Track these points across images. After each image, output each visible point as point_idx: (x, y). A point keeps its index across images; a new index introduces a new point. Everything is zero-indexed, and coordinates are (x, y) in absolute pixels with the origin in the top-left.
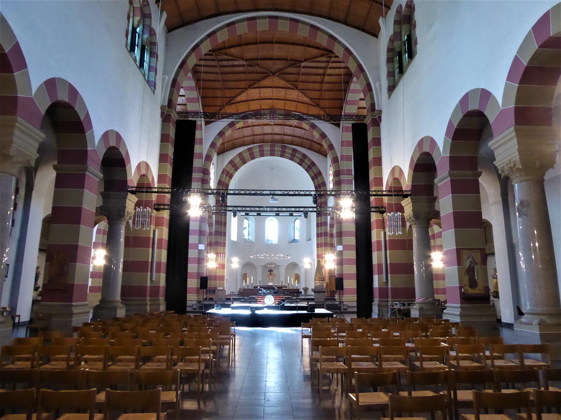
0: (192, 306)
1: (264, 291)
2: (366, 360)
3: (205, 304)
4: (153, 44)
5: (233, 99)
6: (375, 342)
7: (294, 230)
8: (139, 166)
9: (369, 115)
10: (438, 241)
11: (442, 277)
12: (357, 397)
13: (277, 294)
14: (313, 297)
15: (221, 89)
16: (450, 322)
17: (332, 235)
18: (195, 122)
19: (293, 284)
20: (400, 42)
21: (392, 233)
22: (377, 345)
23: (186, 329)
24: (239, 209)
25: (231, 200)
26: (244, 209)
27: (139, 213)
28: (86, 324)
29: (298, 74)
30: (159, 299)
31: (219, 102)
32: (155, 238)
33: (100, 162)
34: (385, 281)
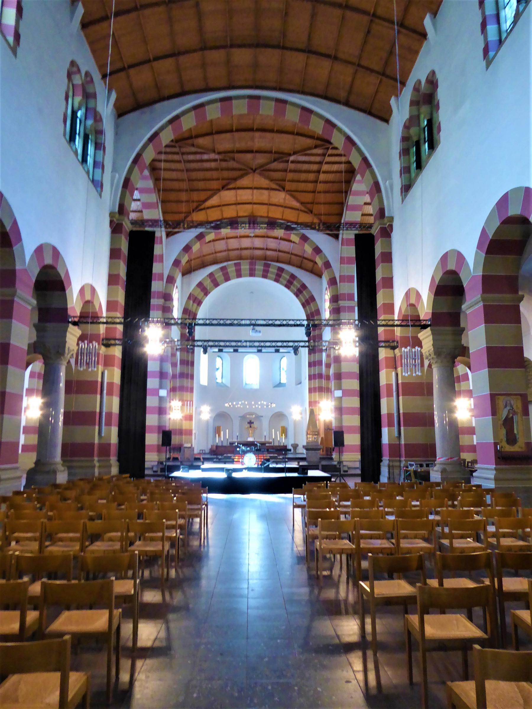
0: (152, 468)
1: (243, 448)
2: (378, 537)
3: (168, 466)
4: (99, 132)
6: (388, 513)
8: (82, 291)
9: (377, 223)
10: (463, 386)
11: (471, 431)
12: (372, 587)
13: (260, 452)
14: (305, 456)
15: (187, 190)
16: (483, 488)
17: (328, 378)
18: (153, 233)
19: (279, 439)
20: (418, 128)
21: (409, 373)
22: (392, 518)
23: (145, 497)
24: (211, 344)
25: (199, 333)
26: (217, 344)
27: (83, 349)
28: (18, 493)
29: (285, 171)
30: (110, 460)
31: (184, 208)
33: (32, 285)
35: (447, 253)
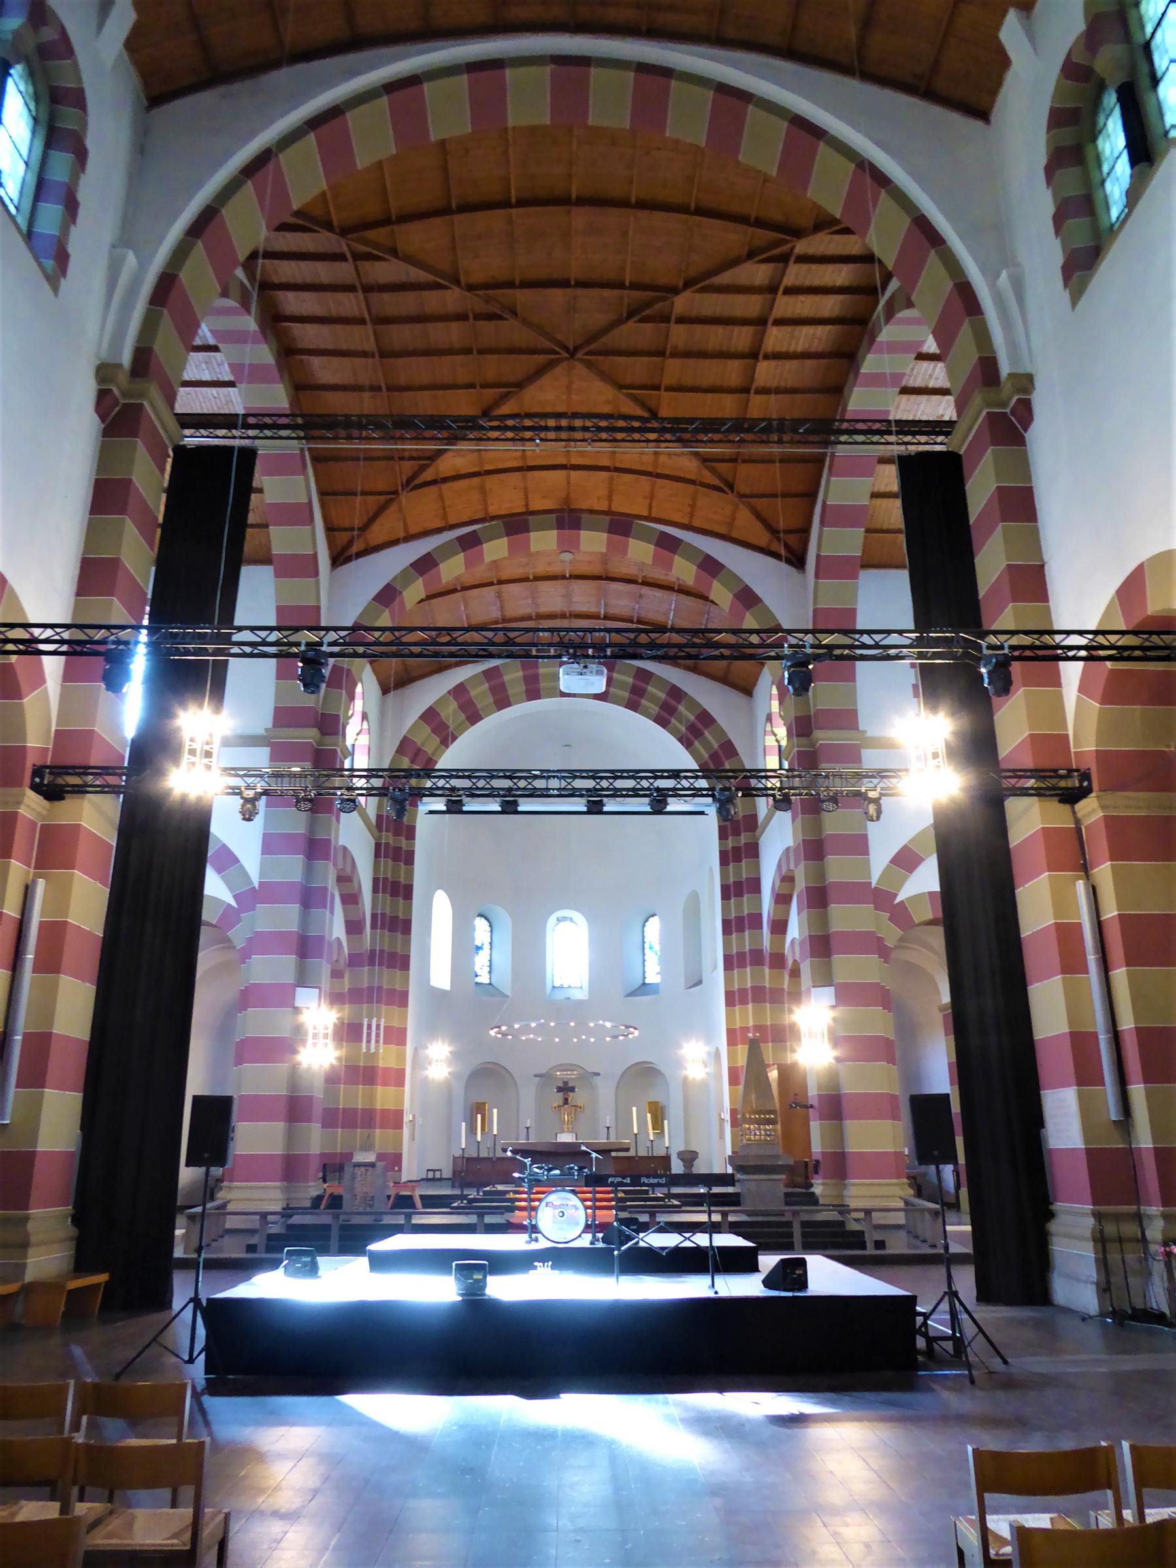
5: (428, 466)
7: (644, 954)
32: (29, 922)
34: (1114, 1115)
35: (1140, 568)
